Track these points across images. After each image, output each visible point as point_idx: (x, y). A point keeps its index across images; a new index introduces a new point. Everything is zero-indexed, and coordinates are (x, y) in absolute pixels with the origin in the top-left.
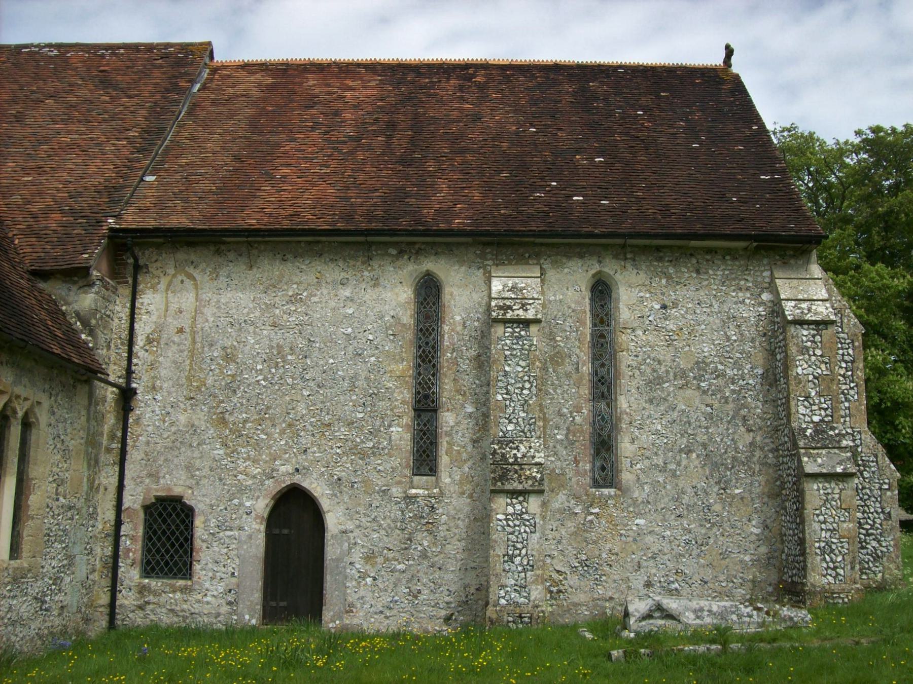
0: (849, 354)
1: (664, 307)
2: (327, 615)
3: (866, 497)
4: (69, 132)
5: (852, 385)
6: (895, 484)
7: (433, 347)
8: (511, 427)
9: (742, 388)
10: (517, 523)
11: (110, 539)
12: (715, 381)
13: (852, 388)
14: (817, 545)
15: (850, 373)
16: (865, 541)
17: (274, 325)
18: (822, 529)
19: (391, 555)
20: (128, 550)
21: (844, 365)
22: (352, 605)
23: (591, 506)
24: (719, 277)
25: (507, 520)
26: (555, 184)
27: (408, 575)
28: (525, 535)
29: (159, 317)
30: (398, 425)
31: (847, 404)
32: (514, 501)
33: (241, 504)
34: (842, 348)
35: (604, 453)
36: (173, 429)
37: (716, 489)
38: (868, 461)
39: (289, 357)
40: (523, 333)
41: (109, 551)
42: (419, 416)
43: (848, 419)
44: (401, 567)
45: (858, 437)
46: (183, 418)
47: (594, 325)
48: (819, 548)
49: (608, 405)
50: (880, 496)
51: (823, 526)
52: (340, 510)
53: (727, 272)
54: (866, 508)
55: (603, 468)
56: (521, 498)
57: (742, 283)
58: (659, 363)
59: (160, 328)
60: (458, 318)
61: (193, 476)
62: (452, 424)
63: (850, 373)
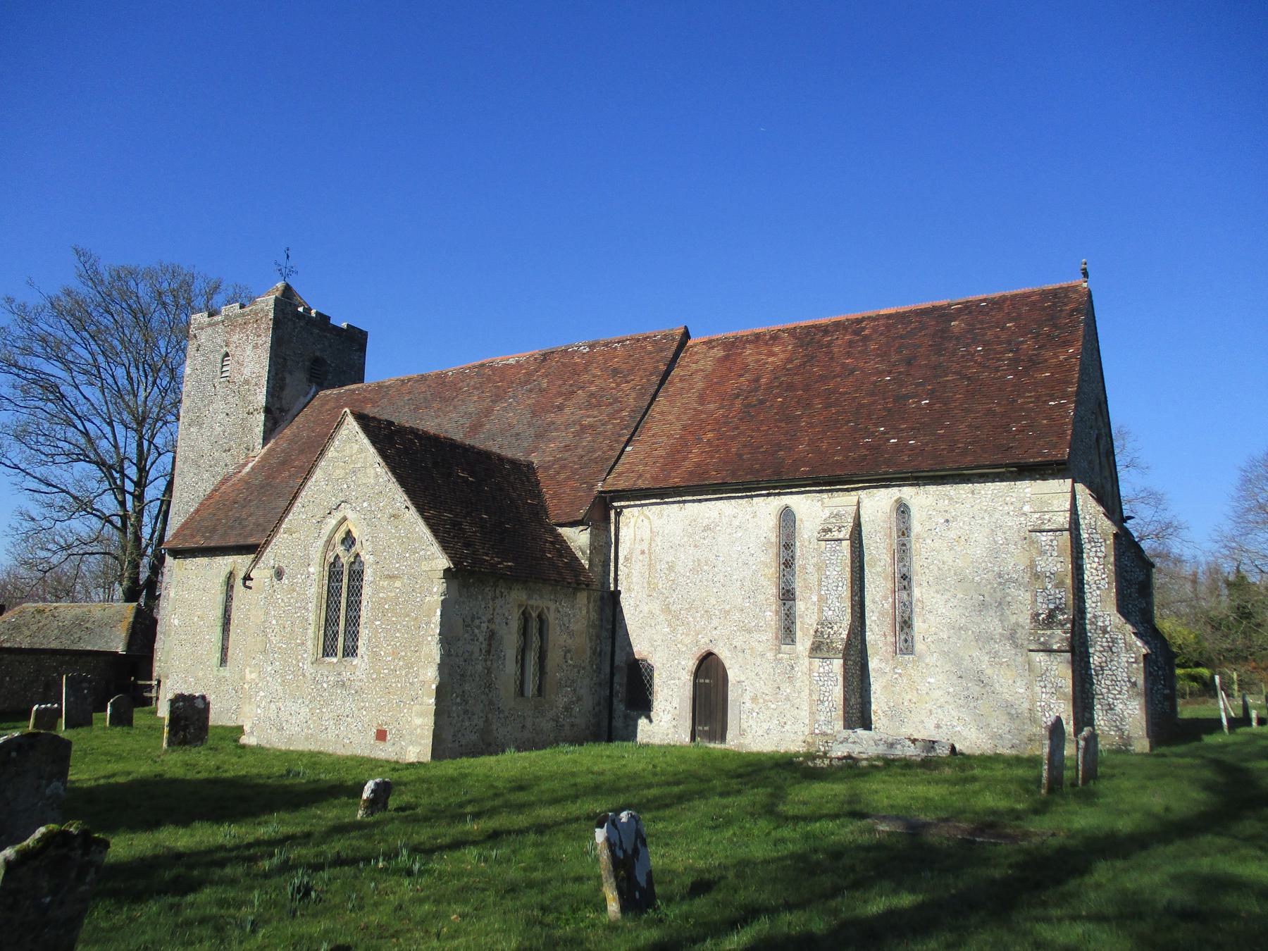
0: (1101, 551)
1: (947, 521)
2: (729, 736)
3: (1115, 668)
4: (588, 416)
5: (1104, 576)
6: (1141, 658)
7: (792, 557)
8: (831, 613)
9: (1007, 580)
10: (826, 679)
11: (608, 685)
12: (985, 576)
13: (1103, 579)
14: (1039, 704)
15: (1102, 566)
16: (1113, 703)
17: (696, 546)
18: (1043, 692)
19: (767, 698)
20: (618, 692)
21: (1096, 560)
22: (744, 730)
23: (896, 667)
24: (989, 496)
25: (819, 676)
26: (882, 429)
27: (778, 711)
28: (831, 687)
29: (631, 544)
30: (770, 611)
31: (1098, 592)
32: (824, 664)
33: (679, 663)
34: (1095, 547)
35: (906, 630)
36: (641, 615)
37: (987, 658)
38: (1116, 639)
39: (705, 567)
40: (838, 548)
41: (608, 692)
42: (784, 604)
43: (1099, 604)
44: (773, 706)
45: (1108, 619)
46: (646, 609)
47: (899, 537)
48: (1040, 706)
49: (908, 595)
50: (1127, 668)
51: (1044, 690)
52: (737, 666)
53: (995, 491)
54: (1114, 677)
55: (906, 641)
56: (828, 662)
57: (1008, 499)
58: (944, 563)
59: (631, 552)
60: (806, 536)
61: (652, 645)
62: (803, 610)
63: (1102, 566)
